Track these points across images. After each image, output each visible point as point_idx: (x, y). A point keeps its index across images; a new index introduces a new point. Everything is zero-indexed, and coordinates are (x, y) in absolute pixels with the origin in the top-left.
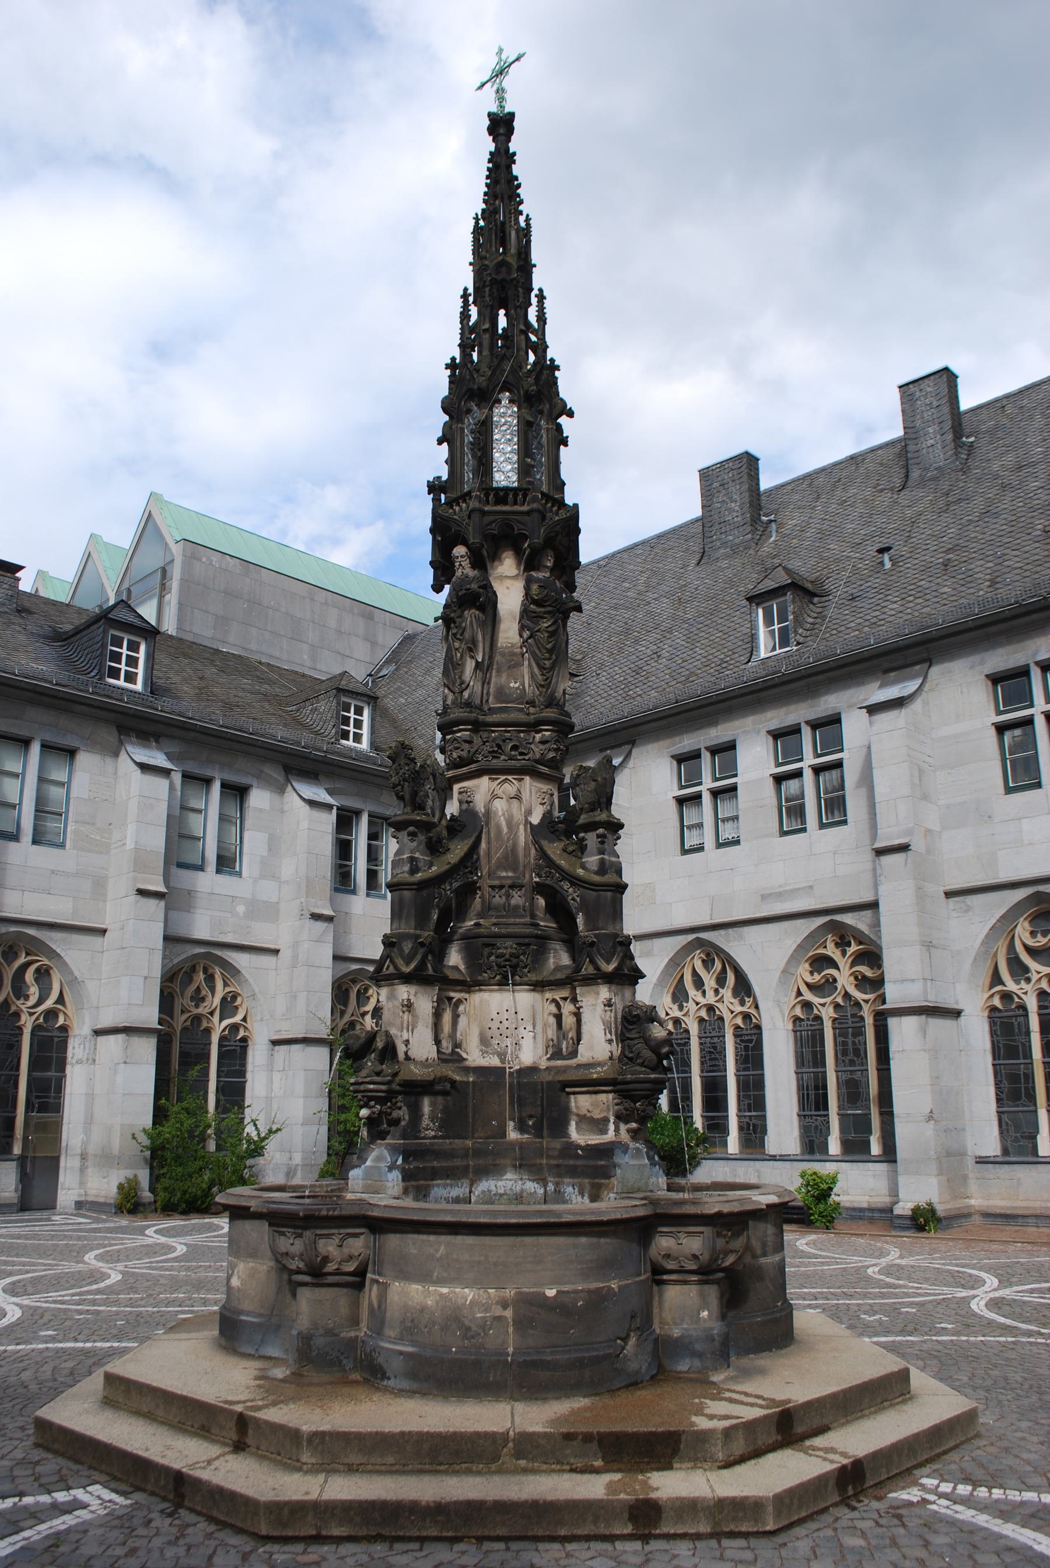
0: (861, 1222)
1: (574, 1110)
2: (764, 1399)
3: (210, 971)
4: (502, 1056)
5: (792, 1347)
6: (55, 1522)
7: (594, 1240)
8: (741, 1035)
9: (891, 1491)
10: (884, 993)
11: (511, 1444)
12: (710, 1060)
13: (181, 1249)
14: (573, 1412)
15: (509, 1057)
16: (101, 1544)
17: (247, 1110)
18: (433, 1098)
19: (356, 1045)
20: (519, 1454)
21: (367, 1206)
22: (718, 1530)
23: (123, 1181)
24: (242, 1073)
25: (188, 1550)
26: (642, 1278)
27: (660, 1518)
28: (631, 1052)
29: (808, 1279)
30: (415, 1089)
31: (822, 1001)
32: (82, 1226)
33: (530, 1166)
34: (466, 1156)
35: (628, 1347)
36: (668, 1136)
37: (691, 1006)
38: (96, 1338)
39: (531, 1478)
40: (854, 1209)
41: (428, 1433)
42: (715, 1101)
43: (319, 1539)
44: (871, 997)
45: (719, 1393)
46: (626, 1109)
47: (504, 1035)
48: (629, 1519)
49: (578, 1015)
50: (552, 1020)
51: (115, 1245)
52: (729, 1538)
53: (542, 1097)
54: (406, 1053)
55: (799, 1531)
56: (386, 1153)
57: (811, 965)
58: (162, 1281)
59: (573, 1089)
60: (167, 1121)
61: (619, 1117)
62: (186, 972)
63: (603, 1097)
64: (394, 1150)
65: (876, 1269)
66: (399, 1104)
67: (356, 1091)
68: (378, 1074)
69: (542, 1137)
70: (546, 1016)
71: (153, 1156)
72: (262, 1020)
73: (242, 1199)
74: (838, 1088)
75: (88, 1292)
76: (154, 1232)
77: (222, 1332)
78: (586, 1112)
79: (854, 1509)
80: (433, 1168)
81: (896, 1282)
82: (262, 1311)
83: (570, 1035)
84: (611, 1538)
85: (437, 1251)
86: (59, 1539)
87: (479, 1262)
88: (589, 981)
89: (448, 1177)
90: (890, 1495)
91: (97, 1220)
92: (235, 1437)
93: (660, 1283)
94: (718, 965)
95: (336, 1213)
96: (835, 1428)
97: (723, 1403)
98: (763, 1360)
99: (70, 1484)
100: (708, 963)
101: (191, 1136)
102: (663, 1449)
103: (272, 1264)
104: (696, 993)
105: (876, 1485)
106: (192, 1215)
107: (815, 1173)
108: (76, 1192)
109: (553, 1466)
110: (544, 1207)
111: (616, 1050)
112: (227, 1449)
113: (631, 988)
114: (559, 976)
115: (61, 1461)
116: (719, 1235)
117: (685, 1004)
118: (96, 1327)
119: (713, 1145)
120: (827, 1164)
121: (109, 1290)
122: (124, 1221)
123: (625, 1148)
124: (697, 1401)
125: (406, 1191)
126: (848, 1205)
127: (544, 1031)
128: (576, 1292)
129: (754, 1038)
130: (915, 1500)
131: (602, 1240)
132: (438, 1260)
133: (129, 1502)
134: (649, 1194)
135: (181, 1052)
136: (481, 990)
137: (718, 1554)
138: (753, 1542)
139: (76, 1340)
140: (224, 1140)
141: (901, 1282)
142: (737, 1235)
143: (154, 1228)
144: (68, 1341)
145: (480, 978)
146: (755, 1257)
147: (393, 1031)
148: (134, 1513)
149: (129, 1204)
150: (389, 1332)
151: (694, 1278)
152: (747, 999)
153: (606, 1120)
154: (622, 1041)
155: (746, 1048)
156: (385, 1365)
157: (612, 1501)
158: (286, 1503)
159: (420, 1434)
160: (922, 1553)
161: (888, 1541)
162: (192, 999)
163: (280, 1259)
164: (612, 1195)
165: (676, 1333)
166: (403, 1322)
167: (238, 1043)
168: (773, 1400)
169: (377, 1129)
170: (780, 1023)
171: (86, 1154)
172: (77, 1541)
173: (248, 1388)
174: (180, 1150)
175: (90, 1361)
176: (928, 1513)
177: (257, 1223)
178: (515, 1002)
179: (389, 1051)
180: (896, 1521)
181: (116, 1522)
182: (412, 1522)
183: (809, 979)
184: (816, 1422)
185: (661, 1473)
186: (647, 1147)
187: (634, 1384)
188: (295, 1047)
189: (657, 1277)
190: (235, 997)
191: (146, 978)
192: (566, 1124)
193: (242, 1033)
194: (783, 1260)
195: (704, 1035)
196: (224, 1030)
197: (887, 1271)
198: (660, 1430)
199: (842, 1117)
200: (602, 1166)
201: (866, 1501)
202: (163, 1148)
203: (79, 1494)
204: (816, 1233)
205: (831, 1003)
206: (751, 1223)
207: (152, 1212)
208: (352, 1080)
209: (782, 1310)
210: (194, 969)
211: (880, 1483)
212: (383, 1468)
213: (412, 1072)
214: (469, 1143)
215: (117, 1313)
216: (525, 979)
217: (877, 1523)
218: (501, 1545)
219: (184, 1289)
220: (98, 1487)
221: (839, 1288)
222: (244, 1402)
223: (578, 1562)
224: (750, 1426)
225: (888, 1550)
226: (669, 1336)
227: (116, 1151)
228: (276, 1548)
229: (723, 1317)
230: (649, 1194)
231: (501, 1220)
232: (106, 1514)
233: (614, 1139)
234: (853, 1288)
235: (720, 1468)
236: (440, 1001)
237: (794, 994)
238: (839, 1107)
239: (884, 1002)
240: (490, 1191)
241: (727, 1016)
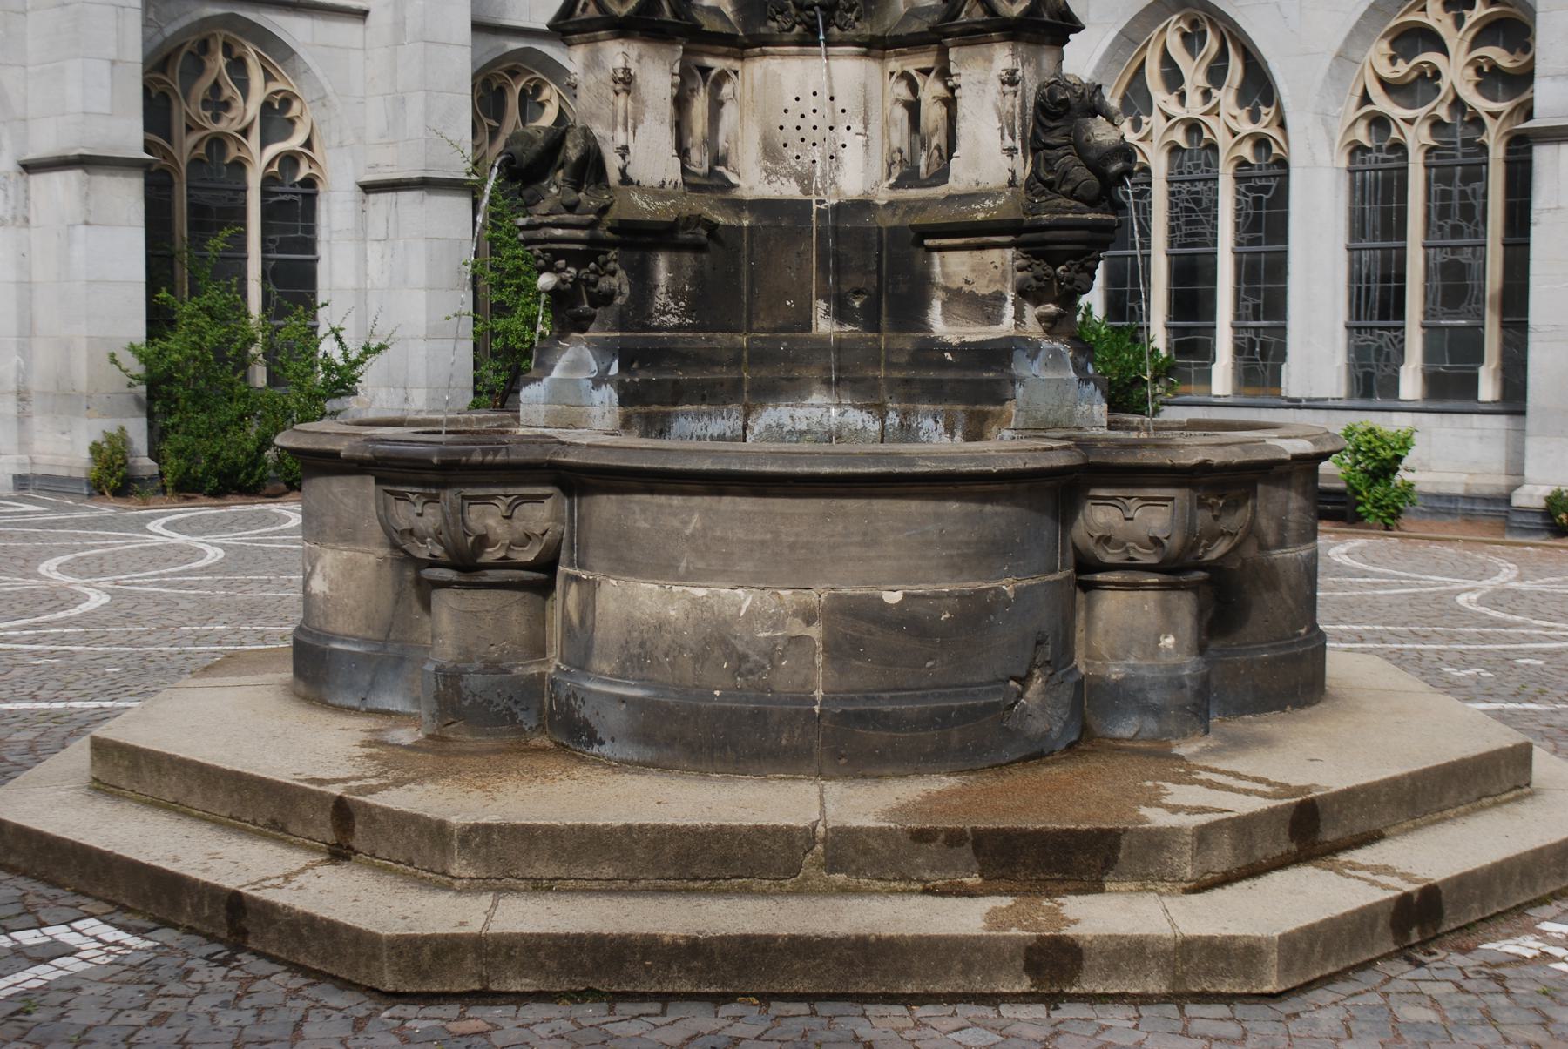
0: (1449, 519)
1: (939, 279)
2: (1269, 784)
3: (237, 51)
4: (805, 180)
5: (1321, 705)
6: (20, 977)
7: (973, 507)
8: (1249, 179)
9: (1486, 940)
10: (1532, 100)
11: (819, 848)
12: (1188, 223)
13: (214, 554)
14: (929, 798)
15: (817, 181)
16: (104, 1008)
17: (321, 313)
18: (674, 256)
19: (527, 155)
20: (833, 863)
21: (557, 447)
22: (1182, 989)
23: (100, 438)
24: (309, 245)
25: (259, 1015)
26: (1059, 576)
27: (1080, 967)
28: (1052, 171)
29: (1348, 609)
30: (642, 239)
31: (1409, 114)
32: (31, 518)
33: (855, 381)
34: (736, 362)
35: (1028, 695)
36: (1103, 362)
37: (1156, 122)
38: (71, 694)
39: (855, 902)
40: (1438, 497)
41: (672, 827)
42: (1191, 298)
43: (485, 996)
44: (1504, 106)
45: (1189, 773)
46: (1037, 278)
47: (809, 141)
48: (1025, 969)
49: (950, 103)
50: (901, 114)
51: (93, 547)
52: (1198, 1003)
53: (880, 256)
54: (623, 171)
55: (1321, 995)
56: (588, 355)
57: (1392, 44)
58: (184, 605)
59: (938, 242)
60: (174, 331)
61: (1024, 293)
62: (190, 53)
63: (994, 255)
64: (603, 349)
65: (1474, 597)
66: (611, 266)
67: (528, 242)
68: (571, 208)
69: (878, 330)
70: (888, 105)
71: (152, 395)
72: (341, 145)
73: (324, 438)
74: (1427, 277)
75: (50, 624)
76: (163, 525)
77: (298, 672)
78: (961, 283)
79: (1420, 964)
80: (676, 382)
81: (1509, 617)
82: (370, 634)
83: (935, 142)
84: (993, 999)
85: (685, 523)
86: (29, 1001)
87: (763, 543)
88: (975, 35)
89: (703, 400)
90: (1484, 946)
91: (58, 508)
92: (331, 838)
93: (1090, 587)
94: (1212, 44)
95: (499, 458)
96: (1392, 836)
97: (1197, 787)
98: (1269, 724)
99: (43, 919)
100: (1192, 40)
101: (221, 358)
102: (1088, 858)
103: (384, 551)
104: (1166, 97)
105: (1460, 929)
106: (231, 499)
107: (1371, 431)
108: (13, 458)
109: (893, 884)
110: (882, 448)
111: (1023, 168)
112: (318, 858)
113: (1054, 52)
114: (916, 27)
115: (22, 882)
116: (1202, 504)
117: (1144, 119)
118: (69, 678)
119: (1185, 379)
120: (1395, 415)
121: (89, 619)
122: (107, 509)
123: (1033, 350)
124: (1149, 784)
125: (626, 424)
126: (1428, 489)
127: (886, 134)
128: (937, 596)
129: (1273, 183)
130: (1529, 954)
131: (988, 508)
132: (687, 539)
133: (150, 944)
134: (1076, 433)
135: (190, 205)
136: (764, 54)
137: (1178, 1026)
138: (1240, 1010)
139: (35, 698)
140: (282, 365)
141: (1518, 618)
142: (1234, 505)
143: (163, 521)
144: (20, 700)
145: (763, 30)
146: (1263, 547)
147: (598, 130)
148: (160, 960)
149: (113, 479)
150: (602, 665)
151: (1153, 579)
152: (1264, 110)
153: (999, 298)
154: (1034, 151)
155: (1257, 202)
156: (593, 721)
157: (997, 939)
158: (427, 939)
159: (659, 829)
160: (1538, 1036)
161: (1477, 1016)
162: (206, 104)
163: (399, 543)
164: (1007, 434)
165: (1116, 672)
166: (625, 646)
167: (298, 189)
168: (1285, 786)
169: (569, 311)
170: (1324, 156)
171: (27, 392)
172: (63, 1004)
173: (350, 759)
174: (202, 383)
175: (62, 731)
176: (1550, 974)
177: (354, 480)
178: (830, 77)
179: (591, 167)
180: (1493, 986)
181: (129, 975)
182: (648, 969)
183: (1388, 72)
184: (1361, 825)
185: (1082, 898)
186: (1074, 349)
187: (1037, 755)
188: (406, 197)
189: (1083, 578)
190: (287, 102)
191: (113, 63)
192: (923, 304)
193: (304, 171)
194: (1314, 556)
195: (1177, 177)
196: (270, 165)
197: (1494, 599)
198: (1084, 827)
199: (1429, 330)
200: (989, 381)
201: (1442, 954)
202: (170, 379)
203: (61, 933)
204: (1365, 535)
205: (1426, 118)
206: (1260, 487)
207: (156, 492)
208: (522, 221)
209: (1306, 642)
210: (204, 47)
211: (1467, 927)
212: (595, 885)
213: (635, 206)
214: (742, 340)
215: (106, 656)
216: (851, 33)
217: (1459, 987)
218: (803, 1008)
219: (224, 617)
220: (92, 921)
221: (1405, 624)
222: (344, 781)
223: (936, 1034)
224: (1243, 826)
225: (1477, 1030)
226: (1101, 678)
227: (82, 384)
228: (411, 1010)
229: (1201, 649)
230: (1076, 433)
231: (802, 469)
232: (110, 964)
233: (1013, 332)
234: (1430, 625)
235: (1186, 891)
236: (686, 74)
237: (1356, 100)
238: (1426, 314)
239: (1529, 115)
240: (781, 426)
241: (1224, 141)
